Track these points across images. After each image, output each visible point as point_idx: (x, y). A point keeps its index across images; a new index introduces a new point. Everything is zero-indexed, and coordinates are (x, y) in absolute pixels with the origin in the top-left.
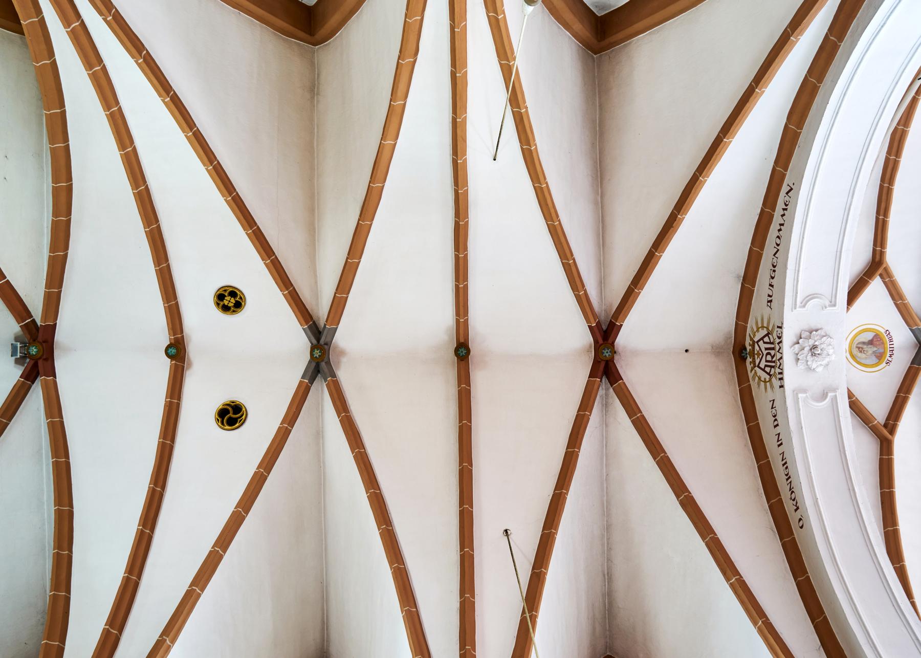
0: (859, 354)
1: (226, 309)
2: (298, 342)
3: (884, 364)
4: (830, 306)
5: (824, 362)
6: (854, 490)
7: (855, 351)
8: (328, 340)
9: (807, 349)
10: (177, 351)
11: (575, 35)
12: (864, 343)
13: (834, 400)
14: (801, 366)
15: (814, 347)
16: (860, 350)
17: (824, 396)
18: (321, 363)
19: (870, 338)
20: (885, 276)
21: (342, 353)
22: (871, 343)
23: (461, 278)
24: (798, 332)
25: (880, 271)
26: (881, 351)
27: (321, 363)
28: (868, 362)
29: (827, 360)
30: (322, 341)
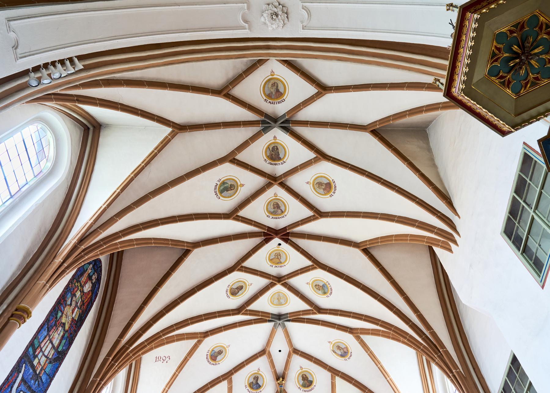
0: (270, 84)
3: (265, 98)
4: (303, 26)
5: (267, 22)
6: (187, 32)
7: (272, 82)
9: (275, 10)
12: (277, 86)
13: (244, 28)
14: (264, 7)
15: (277, 15)
16: (273, 85)
17: (246, 21)
19: (280, 91)
20: (314, 217)
22: (278, 91)
23: (342, 375)
24: (286, 5)
25: (317, 215)
26: (273, 97)
28: (266, 88)
29: (269, 24)
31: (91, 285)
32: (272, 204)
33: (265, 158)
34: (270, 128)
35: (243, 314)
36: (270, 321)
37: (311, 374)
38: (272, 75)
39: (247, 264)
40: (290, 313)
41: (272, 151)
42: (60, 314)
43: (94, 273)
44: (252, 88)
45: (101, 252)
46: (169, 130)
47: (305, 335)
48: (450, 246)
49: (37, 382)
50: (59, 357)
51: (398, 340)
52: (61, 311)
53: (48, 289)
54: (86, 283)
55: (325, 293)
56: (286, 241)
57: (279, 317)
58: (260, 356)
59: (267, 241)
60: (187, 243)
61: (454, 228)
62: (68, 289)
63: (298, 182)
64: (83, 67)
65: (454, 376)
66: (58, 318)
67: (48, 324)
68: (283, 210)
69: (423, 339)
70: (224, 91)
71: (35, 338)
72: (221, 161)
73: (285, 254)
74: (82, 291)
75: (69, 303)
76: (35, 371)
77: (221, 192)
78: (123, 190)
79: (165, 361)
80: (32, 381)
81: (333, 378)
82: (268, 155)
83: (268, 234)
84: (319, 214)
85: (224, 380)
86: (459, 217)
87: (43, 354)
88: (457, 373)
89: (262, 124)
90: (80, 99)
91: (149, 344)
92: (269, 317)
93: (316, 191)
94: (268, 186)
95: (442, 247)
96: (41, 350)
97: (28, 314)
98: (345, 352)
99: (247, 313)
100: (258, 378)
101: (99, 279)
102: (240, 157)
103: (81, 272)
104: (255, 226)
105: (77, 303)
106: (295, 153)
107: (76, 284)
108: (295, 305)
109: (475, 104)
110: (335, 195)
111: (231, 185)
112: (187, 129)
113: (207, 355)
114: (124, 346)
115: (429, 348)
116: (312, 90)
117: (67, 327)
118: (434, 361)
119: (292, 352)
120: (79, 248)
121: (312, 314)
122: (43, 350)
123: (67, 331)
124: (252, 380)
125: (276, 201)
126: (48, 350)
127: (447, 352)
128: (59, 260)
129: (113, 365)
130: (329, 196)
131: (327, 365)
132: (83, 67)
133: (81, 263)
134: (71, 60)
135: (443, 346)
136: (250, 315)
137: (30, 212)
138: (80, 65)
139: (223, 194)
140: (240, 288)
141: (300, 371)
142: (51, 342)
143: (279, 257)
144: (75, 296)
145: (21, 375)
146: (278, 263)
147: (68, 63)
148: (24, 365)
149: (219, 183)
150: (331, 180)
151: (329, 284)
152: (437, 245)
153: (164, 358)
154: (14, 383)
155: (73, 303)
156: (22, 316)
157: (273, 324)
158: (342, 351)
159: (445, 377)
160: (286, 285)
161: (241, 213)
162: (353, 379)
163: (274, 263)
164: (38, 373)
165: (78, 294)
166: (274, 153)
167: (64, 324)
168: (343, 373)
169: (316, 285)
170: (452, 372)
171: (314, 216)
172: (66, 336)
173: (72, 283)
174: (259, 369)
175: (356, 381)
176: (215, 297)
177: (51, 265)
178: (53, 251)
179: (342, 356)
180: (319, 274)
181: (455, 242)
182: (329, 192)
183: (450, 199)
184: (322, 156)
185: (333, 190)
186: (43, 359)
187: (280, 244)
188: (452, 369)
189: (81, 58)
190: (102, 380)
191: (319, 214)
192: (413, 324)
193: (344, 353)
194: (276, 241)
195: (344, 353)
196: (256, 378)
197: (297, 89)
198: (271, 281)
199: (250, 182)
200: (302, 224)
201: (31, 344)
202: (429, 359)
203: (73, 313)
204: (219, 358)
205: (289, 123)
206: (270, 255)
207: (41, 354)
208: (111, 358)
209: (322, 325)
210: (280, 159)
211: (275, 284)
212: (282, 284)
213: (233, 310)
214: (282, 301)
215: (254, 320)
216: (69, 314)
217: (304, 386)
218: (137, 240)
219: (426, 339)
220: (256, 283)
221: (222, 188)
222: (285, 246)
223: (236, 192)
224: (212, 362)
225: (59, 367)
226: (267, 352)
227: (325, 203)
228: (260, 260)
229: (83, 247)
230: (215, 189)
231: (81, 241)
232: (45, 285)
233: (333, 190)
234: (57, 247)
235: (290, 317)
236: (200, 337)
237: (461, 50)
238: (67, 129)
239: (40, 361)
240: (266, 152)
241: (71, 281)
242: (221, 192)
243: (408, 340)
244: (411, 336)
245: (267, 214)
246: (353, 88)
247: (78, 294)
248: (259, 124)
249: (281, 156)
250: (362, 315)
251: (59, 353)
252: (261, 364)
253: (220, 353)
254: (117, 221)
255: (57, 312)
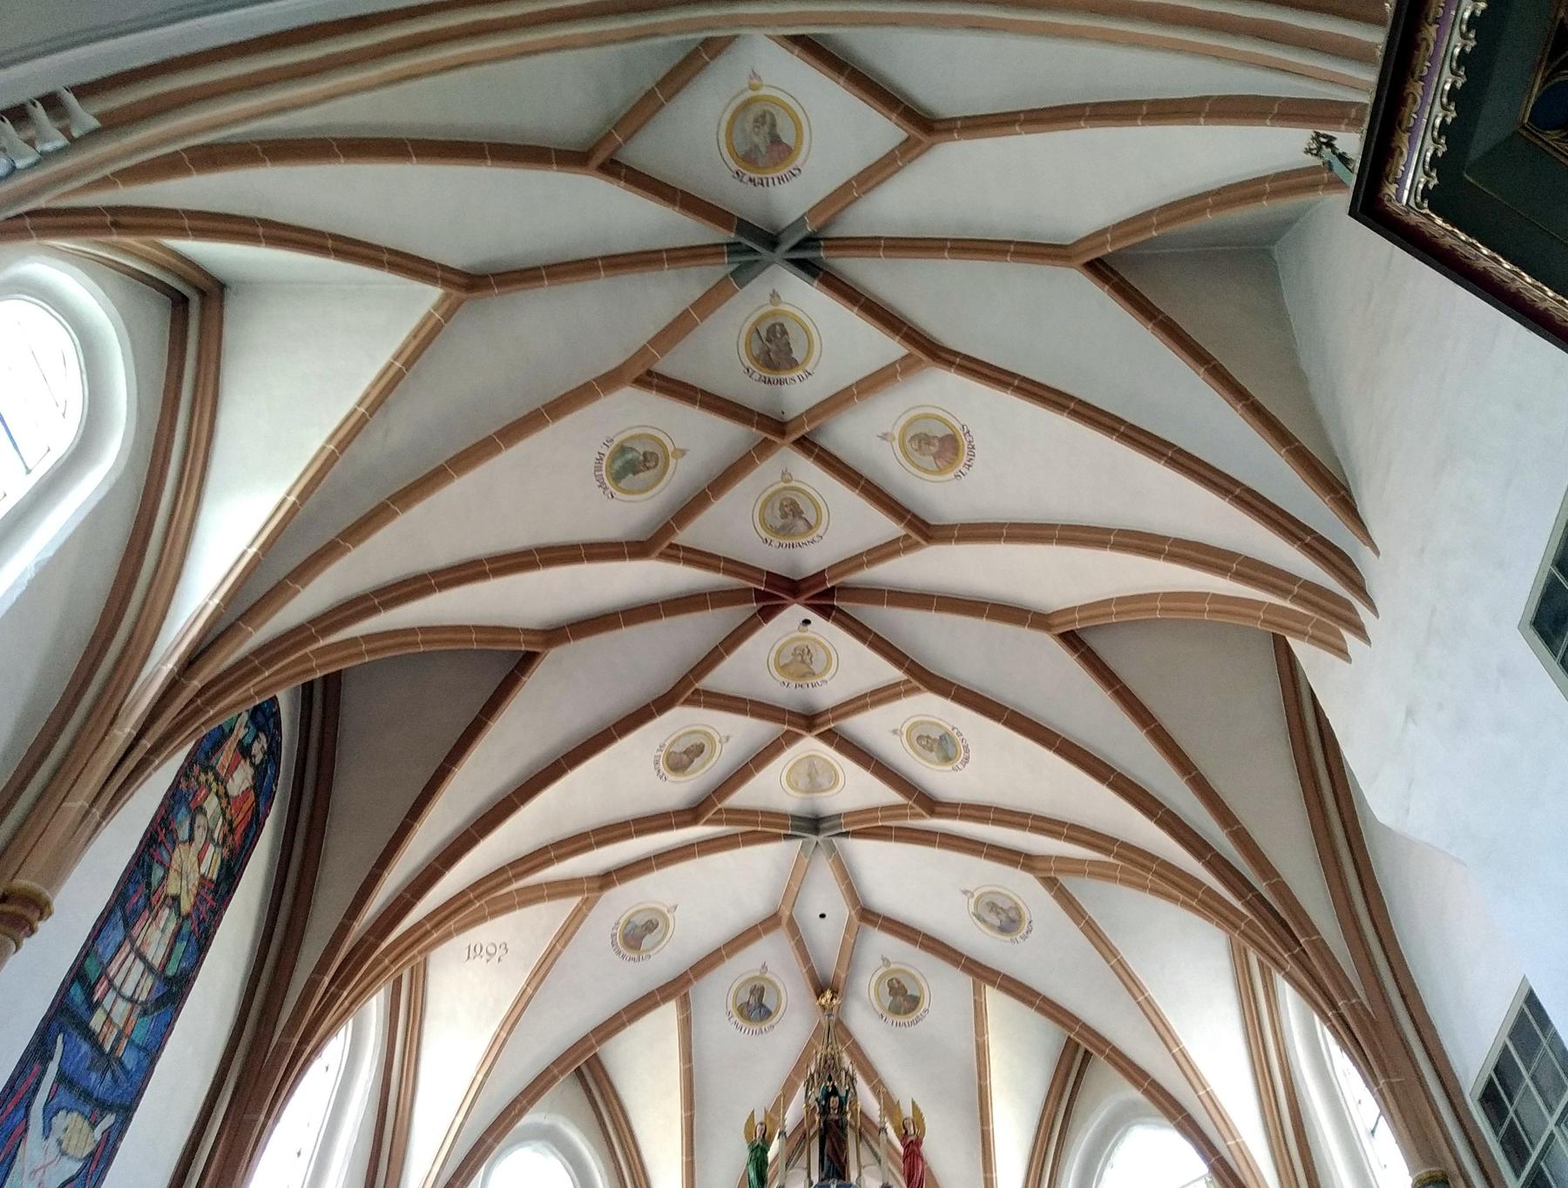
0: (751, 117)
3: (735, 167)
7: (756, 110)
11: (221, 307)
12: (773, 125)
16: (761, 120)
22: (775, 140)
31: (250, 771)
32: (777, 505)
33: (748, 363)
34: (757, 266)
35: (709, 822)
36: (787, 837)
37: (913, 977)
38: (753, 88)
39: (711, 681)
40: (848, 814)
41: (769, 340)
42: (158, 873)
43: (256, 737)
44: (694, 135)
45: (258, 688)
46: (432, 294)
47: (896, 874)
48: (1342, 638)
49: (109, 1075)
50: (172, 991)
51: (1174, 899)
52: (162, 864)
53: (99, 825)
54: (232, 768)
55: (947, 759)
56: (826, 611)
57: (813, 824)
58: (767, 931)
59: (767, 613)
60: (526, 631)
61: (1356, 583)
62: (175, 798)
63: (855, 434)
64: (95, 123)
65: (1341, 1017)
66: (155, 882)
67: (123, 909)
68: (812, 522)
69: (1247, 904)
70: (600, 155)
71: (87, 955)
72: (609, 381)
73: (824, 647)
74: (224, 796)
75: (183, 834)
76: (97, 1045)
77: (617, 477)
78: (409, 364)
79: (496, 958)
80: (94, 1076)
81: (978, 992)
82: (756, 352)
83: (771, 593)
84: (924, 530)
85: (665, 1000)
86: (1377, 553)
87: (119, 994)
88: (1352, 1008)
89: (730, 253)
90: (124, 219)
91: (436, 927)
92: (785, 827)
93: (913, 464)
94: (763, 449)
95: (1315, 640)
96: (111, 983)
97: (39, 906)
98: (1013, 921)
99: (719, 814)
100: (762, 990)
101: (273, 752)
102: (669, 365)
103: (203, 758)
104: (726, 572)
105: (210, 831)
106: (837, 341)
107: (203, 778)
108: (856, 789)
109: (1472, 245)
110: (971, 473)
111: (645, 454)
112: (489, 286)
113: (613, 936)
114: (362, 941)
115: (1268, 929)
116: (885, 132)
117: (186, 906)
118: (1280, 967)
119: (856, 920)
120: (184, 687)
121: (916, 814)
122: (117, 982)
123: (189, 916)
124: (745, 996)
125: (789, 494)
126: (132, 979)
127: (1322, 948)
128: (125, 730)
129: (335, 997)
130: (951, 475)
131: (962, 955)
132: (95, 123)
133: (202, 728)
134: (51, 102)
135: (1309, 927)
136: (729, 822)
137: (18, 592)
138: (85, 117)
139: (621, 484)
140: (699, 750)
141: (884, 969)
142: (141, 956)
143: (807, 658)
144: (200, 810)
145: (53, 1068)
146: (804, 676)
147: (39, 112)
148: (60, 1039)
149: (607, 452)
150: (958, 427)
151: (959, 734)
152: (1301, 634)
153: (491, 950)
154: (35, 1091)
155: (200, 835)
156: (23, 917)
157: (800, 842)
158: (1003, 917)
159: (1309, 1008)
160: (831, 737)
161: (684, 537)
162: (1036, 994)
163: (791, 675)
164: (107, 1049)
165: (212, 805)
166: (772, 347)
167: (176, 899)
168: (1006, 978)
169: (920, 738)
170: (1334, 1006)
171: (907, 537)
172: (185, 930)
173: (187, 777)
174: (764, 966)
175: (1045, 1000)
176: (628, 776)
177: (98, 754)
178: (107, 697)
179: (1003, 930)
180: (930, 707)
181: (1359, 630)
182: (952, 463)
183: (1348, 490)
184: (929, 349)
185: (965, 459)
186: (122, 1008)
187: (807, 622)
188: (1336, 997)
189: (84, 91)
190: (305, 1040)
191: (924, 530)
192: (1218, 856)
193: (1010, 922)
194: (795, 612)
195: (1010, 922)
196: (759, 992)
197: (837, 131)
198: (786, 727)
199: (699, 439)
200: (871, 563)
201: (78, 974)
202: (1267, 962)
203: (200, 861)
204: (647, 941)
205: (819, 247)
206: (779, 652)
207: (111, 995)
208: (327, 980)
209: (942, 845)
210: (793, 364)
211: (797, 737)
212: (821, 736)
213: (677, 813)
214: (823, 780)
215: (743, 834)
216: (191, 865)
217: (895, 1010)
218: (369, 638)
219: (1258, 903)
220: (736, 734)
221: (619, 463)
222: (823, 628)
223: (664, 473)
224: (629, 954)
225: (169, 1026)
226: (784, 921)
227: (942, 496)
228: (755, 664)
229: (197, 683)
230: (598, 469)
231: (192, 661)
232: (87, 812)
233: (965, 459)
234: (118, 688)
235: (847, 824)
236: (589, 890)
237: (1431, 32)
238: (113, 309)
239: (113, 1015)
240: (748, 344)
241: (184, 773)
242: (617, 477)
243: (1201, 902)
244: (1209, 891)
245: (764, 535)
246: (1024, 123)
247: (212, 805)
248: (721, 254)
249: (797, 354)
250: (1062, 824)
251: (168, 981)
252: (770, 954)
253: (650, 927)
254: (297, 592)
255: (150, 867)
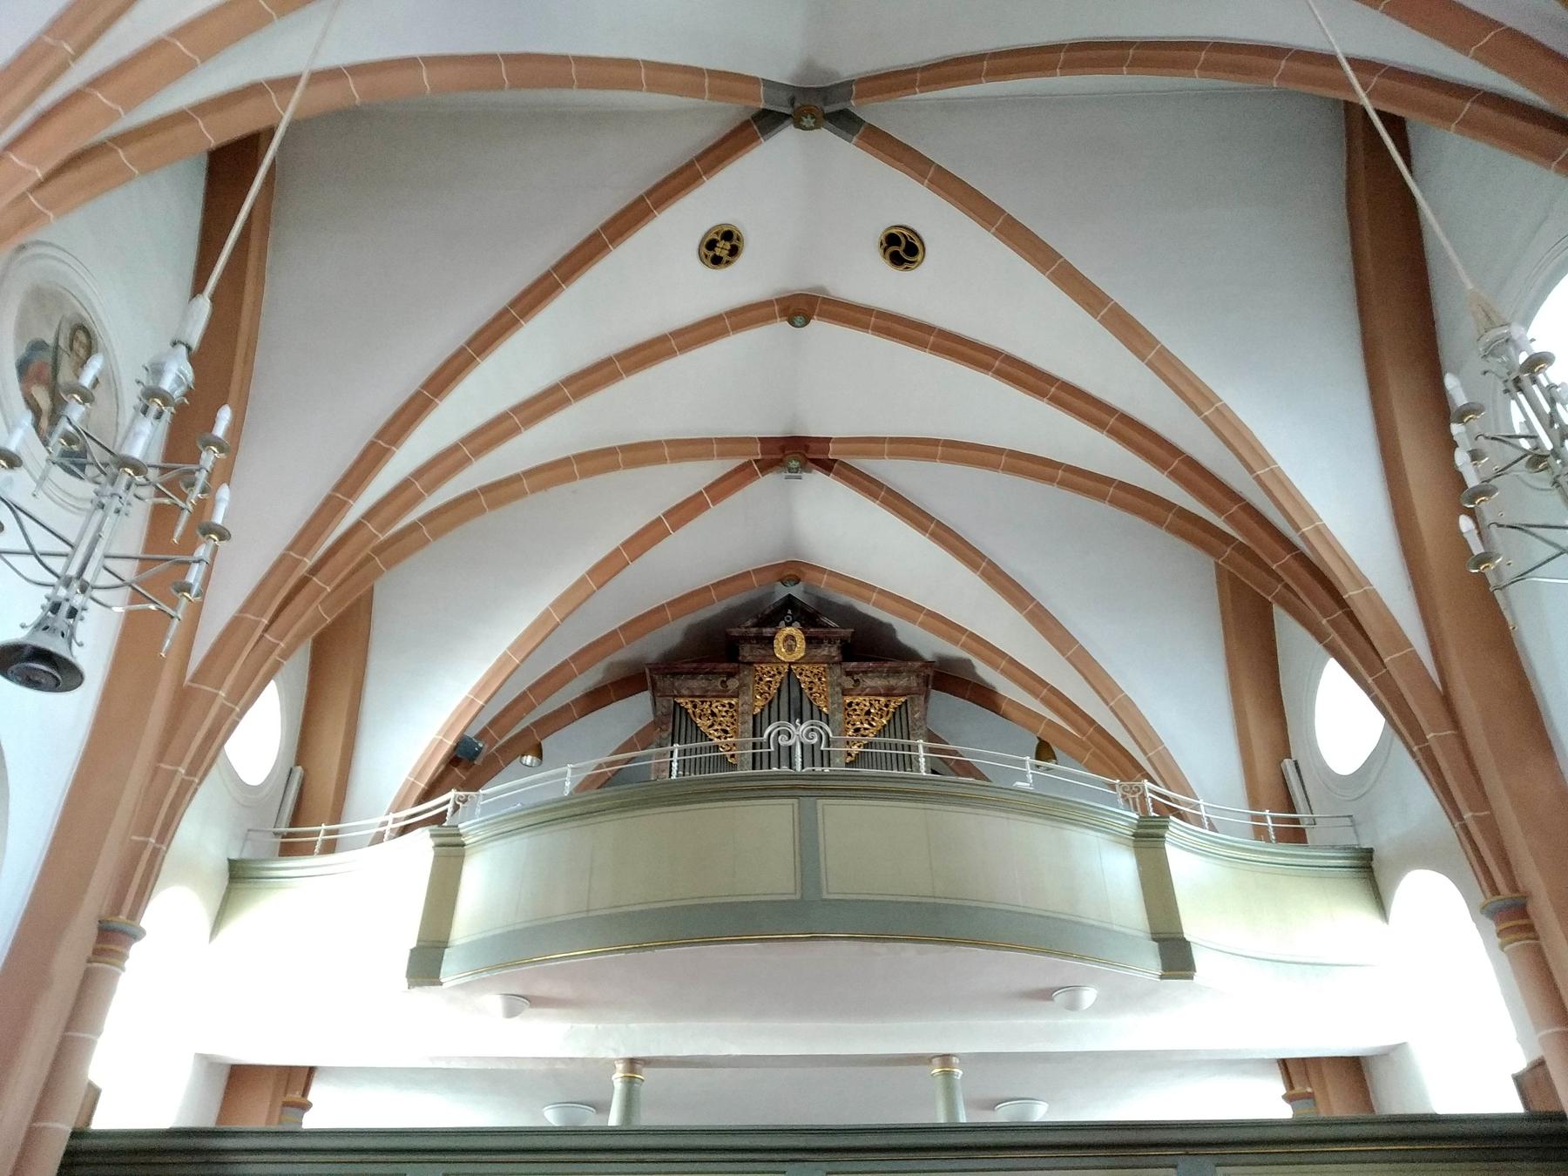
1: (734, 251)
2: (785, 147)
8: (784, 97)
10: (800, 308)
18: (822, 105)
21: (809, 66)
27: (822, 105)
30: (787, 111)
